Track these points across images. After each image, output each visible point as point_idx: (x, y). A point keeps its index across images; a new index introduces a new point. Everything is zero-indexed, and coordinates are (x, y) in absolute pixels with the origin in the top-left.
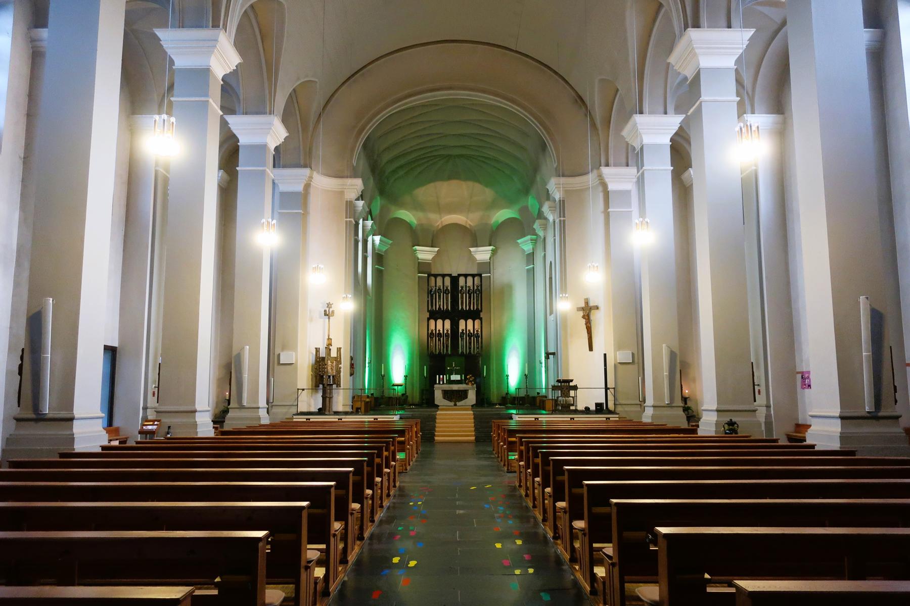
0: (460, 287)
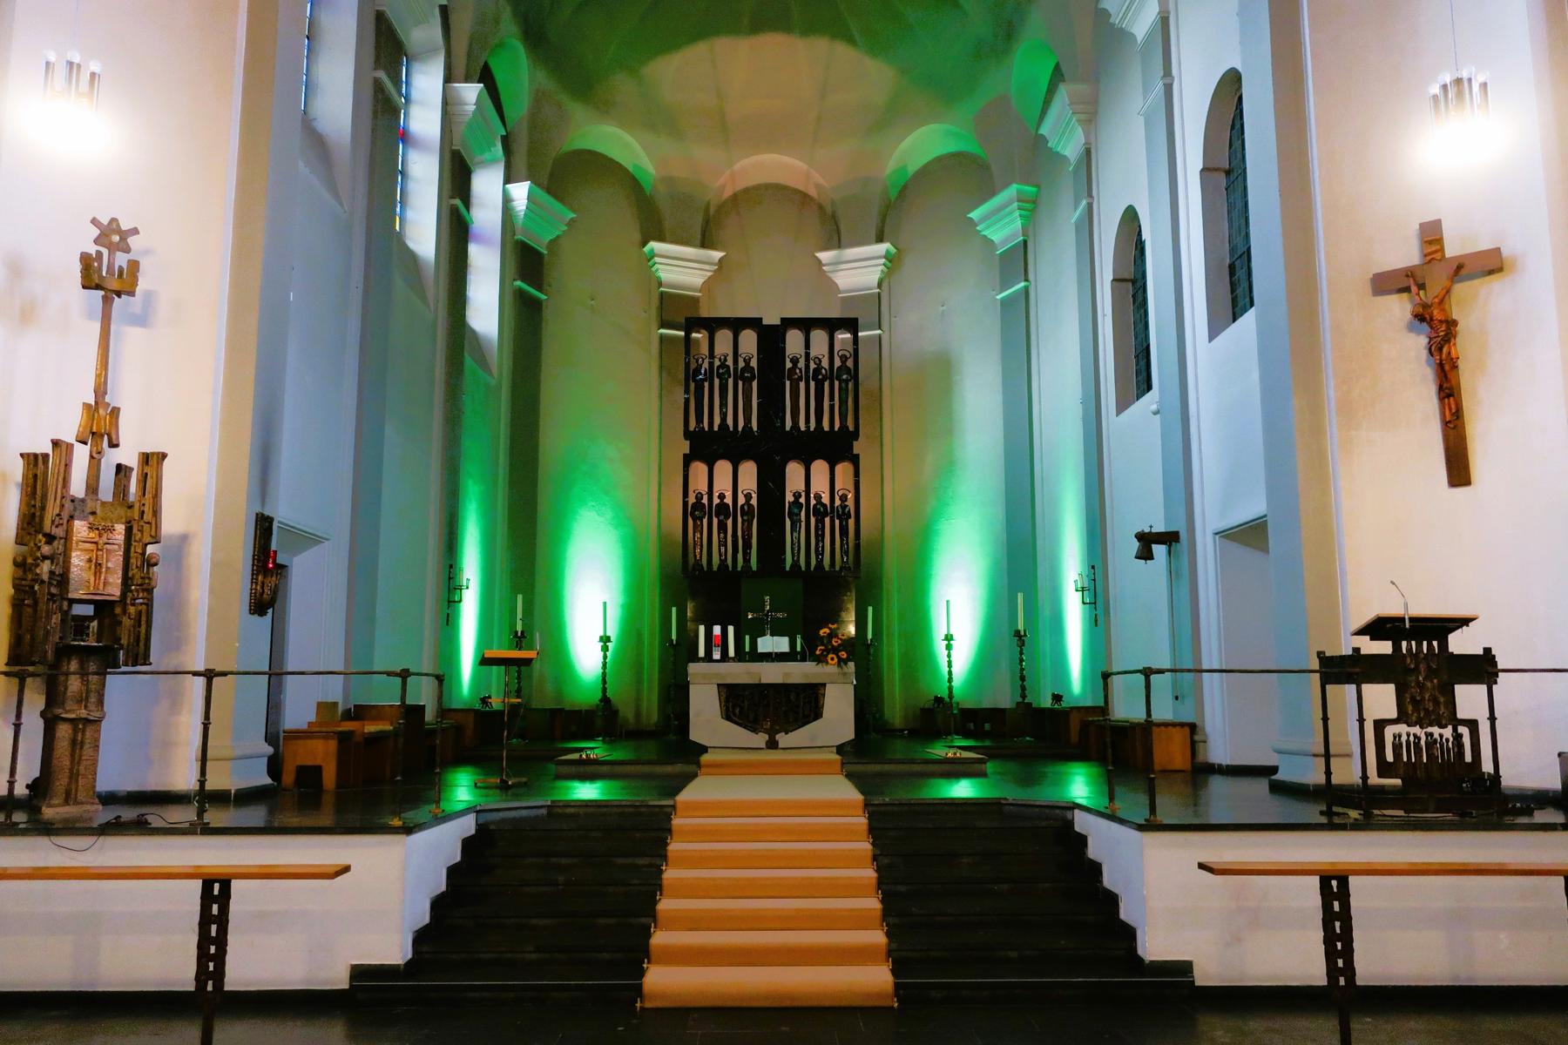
0: (788, 360)
